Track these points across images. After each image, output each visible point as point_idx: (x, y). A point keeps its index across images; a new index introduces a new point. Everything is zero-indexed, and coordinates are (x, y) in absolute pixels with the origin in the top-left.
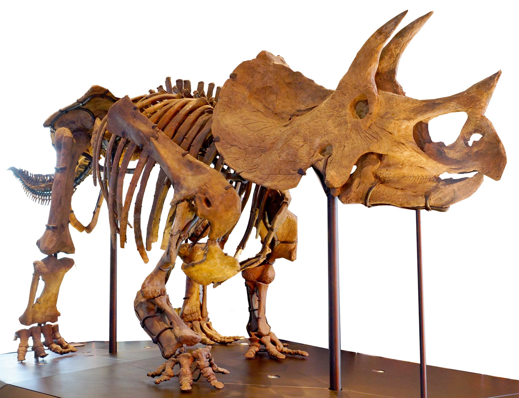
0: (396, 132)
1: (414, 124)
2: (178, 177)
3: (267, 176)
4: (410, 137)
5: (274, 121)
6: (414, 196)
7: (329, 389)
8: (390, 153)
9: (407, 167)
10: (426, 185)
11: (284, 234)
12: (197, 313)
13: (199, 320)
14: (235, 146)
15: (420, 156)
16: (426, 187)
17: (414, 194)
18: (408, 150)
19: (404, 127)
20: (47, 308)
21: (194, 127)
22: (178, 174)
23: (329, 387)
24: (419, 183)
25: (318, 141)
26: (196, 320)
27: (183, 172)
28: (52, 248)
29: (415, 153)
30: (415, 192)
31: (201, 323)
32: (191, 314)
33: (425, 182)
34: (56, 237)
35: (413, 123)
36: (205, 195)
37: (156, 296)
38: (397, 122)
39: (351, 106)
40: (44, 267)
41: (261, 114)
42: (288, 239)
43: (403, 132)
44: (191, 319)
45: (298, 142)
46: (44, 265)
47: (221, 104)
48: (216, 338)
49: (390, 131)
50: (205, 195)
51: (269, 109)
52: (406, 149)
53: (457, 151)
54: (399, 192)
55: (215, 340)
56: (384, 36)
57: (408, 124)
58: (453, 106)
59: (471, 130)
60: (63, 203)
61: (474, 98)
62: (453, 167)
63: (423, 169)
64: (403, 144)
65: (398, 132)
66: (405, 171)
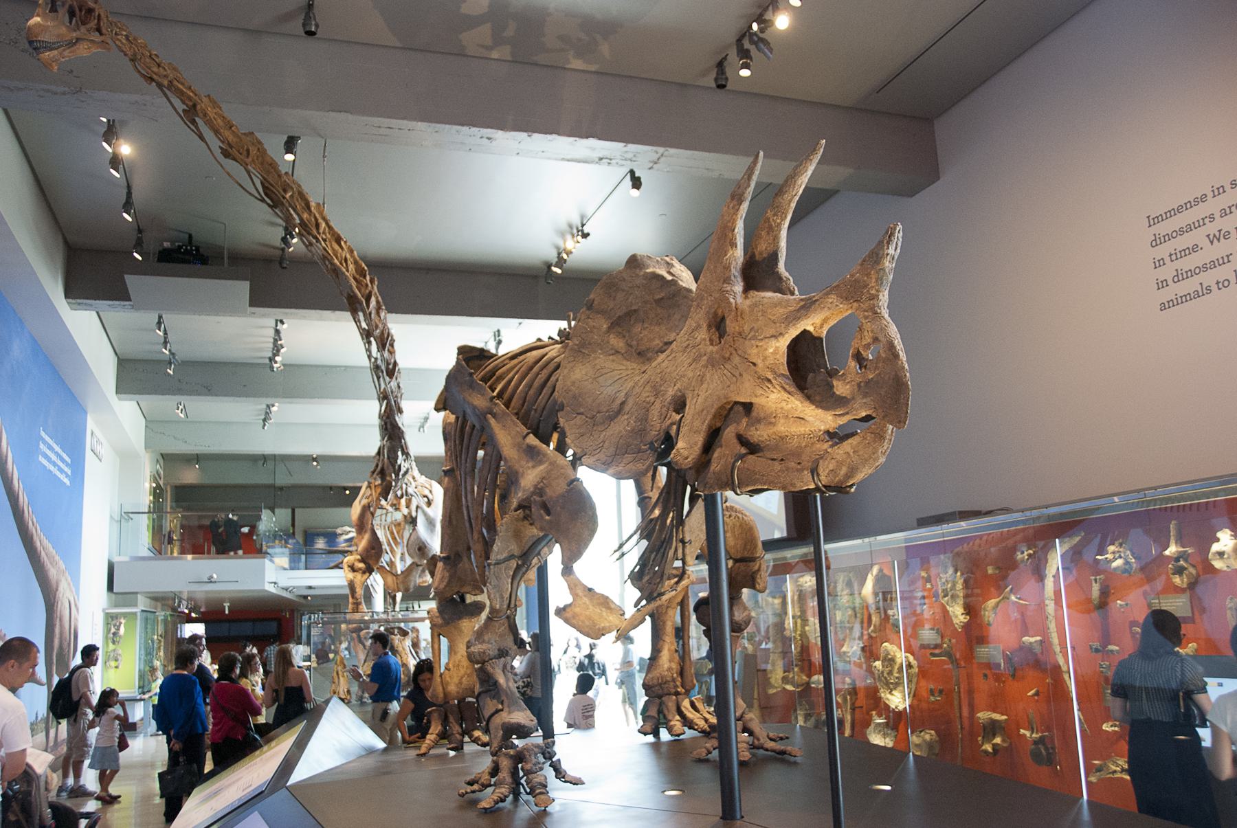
0: (759, 362)
1: (787, 343)
2: (517, 472)
3: (611, 458)
4: (781, 367)
5: (635, 365)
6: (798, 470)
7: (721, 818)
8: (754, 400)
9: (782, 421)
10: (814, 449)
11: (739, 546)
12: (672, 684)
13: (677, 694)
14: (582, 414)
15: (792, 398)
16: (815, 451)
17: (799, 467)
18: (775, 390)
19: (771, 350)
20: (462, 678)
21: (544, 391)
22: (517, 467)
23: (721, 815)
24: (806, 446)
25: (671, 392)
26: (670, 694)
27: (523, 463)
28: (444, 588)
29: (786, 395)
30: (799, 463)
31: (680, 700)
32: (660, 685)
33: (812, 444)
34: (448, 571)
35: (784, 343)
36: (541, 496)
37: (487, 659)
38: (761, 344)
39: (709, 326)
40: (437, 617)
41: (620, 356)
42: (746, 554)
43: (770, 361)
44: (660, 692)
45: (648, 397)
46: (437, 614)
47: (572, 349)
48: (697, 725)
49: (754, 361)
50: (541, 496)
51: (631, 346)
52: (772, 389)
53: (847, 381)
54: (777, 466)
55: (696, 727)
56: (738, 201)
57: (778, 345)
58: (831, 303)
59: (869, 341)
60: (454, 522)
61: (859, 282)
62: (837, 413)
63: (803, 422)
64: (769, 381)
65: (763, 361)
66: (782, 428)
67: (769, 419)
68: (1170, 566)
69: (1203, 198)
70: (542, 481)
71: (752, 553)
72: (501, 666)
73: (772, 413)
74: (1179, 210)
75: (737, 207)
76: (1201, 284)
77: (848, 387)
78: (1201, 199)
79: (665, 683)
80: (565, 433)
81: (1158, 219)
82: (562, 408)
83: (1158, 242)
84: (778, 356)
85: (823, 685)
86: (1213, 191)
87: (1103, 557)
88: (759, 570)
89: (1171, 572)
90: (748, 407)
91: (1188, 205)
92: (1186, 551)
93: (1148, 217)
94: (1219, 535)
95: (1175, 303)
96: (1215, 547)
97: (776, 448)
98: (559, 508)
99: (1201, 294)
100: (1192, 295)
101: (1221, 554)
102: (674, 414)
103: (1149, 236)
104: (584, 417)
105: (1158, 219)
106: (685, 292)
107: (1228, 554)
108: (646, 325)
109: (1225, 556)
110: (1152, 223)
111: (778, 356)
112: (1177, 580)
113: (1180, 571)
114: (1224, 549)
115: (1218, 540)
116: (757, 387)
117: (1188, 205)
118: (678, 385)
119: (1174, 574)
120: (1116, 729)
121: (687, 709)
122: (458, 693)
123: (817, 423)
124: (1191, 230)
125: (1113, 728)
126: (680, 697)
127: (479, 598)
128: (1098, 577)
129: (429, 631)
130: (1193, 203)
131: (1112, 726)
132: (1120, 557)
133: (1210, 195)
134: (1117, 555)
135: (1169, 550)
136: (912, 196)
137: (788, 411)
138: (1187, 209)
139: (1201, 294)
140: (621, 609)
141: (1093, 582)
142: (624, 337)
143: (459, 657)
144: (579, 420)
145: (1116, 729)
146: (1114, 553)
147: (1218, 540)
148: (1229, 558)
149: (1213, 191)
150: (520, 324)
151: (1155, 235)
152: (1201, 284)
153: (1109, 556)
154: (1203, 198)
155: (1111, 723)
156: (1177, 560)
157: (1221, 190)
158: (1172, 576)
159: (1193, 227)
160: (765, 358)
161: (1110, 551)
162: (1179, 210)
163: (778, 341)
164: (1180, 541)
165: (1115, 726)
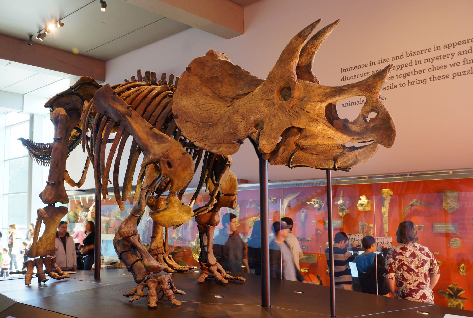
1: (326, 105)
3: (214, 145)
4: (323, 115)
9: (320, 138)
13: (163, 254)
14: (190, 122)
16: (335, 153)
17: (326, 158)
18: (320, 125)
19: (318, 107)
20: (48, 245)
24: (329, 150)
25: (252, 118)
27: (151, 141)
28: (51, 199)
31: (164, 256)
32: (156, 249)
33: (334, 149)
35: (324, 105)
36: (167, 159)
37: (130, 235)
38: (312, 104)
40: (45, 214)
41: (209, 97)
42: (230, 192)
43: (317, 112)
44: (156, 253)
45: (238, 119)
46: (45, 212)
48: (176, 268)
52: (319, 124)
53: (358, 125)
54: (314, 157)
55: (175, 269)
57: (321, 105)
58: (355, 92)
60: (59, 166)
62: (355, 138)
63: (332, 140)
64: (317, 120)
65: (313, 111)
66: (319, 141)
67: (314, 136)
68: (338, 208)
69: (366, 65)
70: (167, 151)
71: (233, 192)
72: (137, 238)
73: (315, 134)
74: (355, 68)
75: (302, 41)
76: (361, 99)
77: (359, 128)
78: (365, 65)
79: (158, 249)
80: (181, 130)
81: (346, 70)
82: (177, 117)
83: (344, 79)
84: (321, 110)
85: (328, 248)
86: (370, 63)
87: (310, 203)
88: (235, 199)
89: (338, 210)
90: (300, 130)
91: (359, 67)
92: (345, 203)
93: (341, 69)
94: (361, 197)
95: (349, 105)
96: (360, 202)
97: (313, 149)
98: (177, 165)
99: (360, 103)
100: (356, 103)
101: (362, 205)
102: (254, 128)
103: (341, 76)
104: (191, 123)
105: (346, 70)
106: (246, 73)
107: (365, 205)
108: (223, 85)
109: (364, 206)
110: (343, 71)
111: (321, 110)
112: (341, 214)
113: (342, 210)
114: (364, 203)
115: (360, 199)
116: (311, 122)
117: (359, 67)
118: (259, 116)
119: (339, 211)
120: (307, 271)
121: (168, 260)
122: (44, 252)
123: (340, 141)
124: (359, 77)
125: (305, 271)
126: (164, 255)
127: (65, 205)
128: (304, 211)
129: (36, 220)
130: (361, 67)
131: (304, 270)
132: (317, 203)
133: (369, 64)
134: (316, 203)
135: (339, 202)
136: (228, 39)
137: (325, 134)
138: (358, 68)
139: (360, 103)
140: (274, 213)
141: (302, 213)
142: (210, 88)
143: (50, 234)
144: (189, 124)
145: (307, 271)
146: (314, 201)
147: (360, 199)
148: (365, 206)
149: (370, 63)
150: (9, 63)
151: (343, 76)
152: (361, 99)
153: (312, 203)
154: (366, 65)
155: (304, 269)
156: (342, 206)
157: (374, 64)
158: (339, 212)
159: (360, 76)
160: (314, 111)
161: (313, 201)
162: (355, 68)
163: (322, 104)
164: (343, 200)
165: (306, 270)
